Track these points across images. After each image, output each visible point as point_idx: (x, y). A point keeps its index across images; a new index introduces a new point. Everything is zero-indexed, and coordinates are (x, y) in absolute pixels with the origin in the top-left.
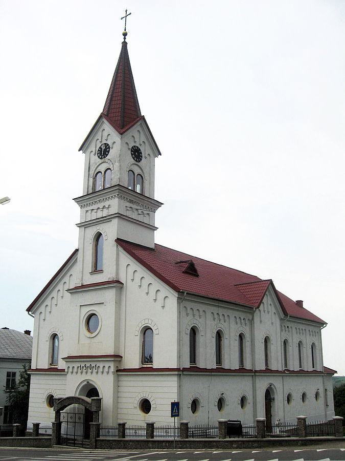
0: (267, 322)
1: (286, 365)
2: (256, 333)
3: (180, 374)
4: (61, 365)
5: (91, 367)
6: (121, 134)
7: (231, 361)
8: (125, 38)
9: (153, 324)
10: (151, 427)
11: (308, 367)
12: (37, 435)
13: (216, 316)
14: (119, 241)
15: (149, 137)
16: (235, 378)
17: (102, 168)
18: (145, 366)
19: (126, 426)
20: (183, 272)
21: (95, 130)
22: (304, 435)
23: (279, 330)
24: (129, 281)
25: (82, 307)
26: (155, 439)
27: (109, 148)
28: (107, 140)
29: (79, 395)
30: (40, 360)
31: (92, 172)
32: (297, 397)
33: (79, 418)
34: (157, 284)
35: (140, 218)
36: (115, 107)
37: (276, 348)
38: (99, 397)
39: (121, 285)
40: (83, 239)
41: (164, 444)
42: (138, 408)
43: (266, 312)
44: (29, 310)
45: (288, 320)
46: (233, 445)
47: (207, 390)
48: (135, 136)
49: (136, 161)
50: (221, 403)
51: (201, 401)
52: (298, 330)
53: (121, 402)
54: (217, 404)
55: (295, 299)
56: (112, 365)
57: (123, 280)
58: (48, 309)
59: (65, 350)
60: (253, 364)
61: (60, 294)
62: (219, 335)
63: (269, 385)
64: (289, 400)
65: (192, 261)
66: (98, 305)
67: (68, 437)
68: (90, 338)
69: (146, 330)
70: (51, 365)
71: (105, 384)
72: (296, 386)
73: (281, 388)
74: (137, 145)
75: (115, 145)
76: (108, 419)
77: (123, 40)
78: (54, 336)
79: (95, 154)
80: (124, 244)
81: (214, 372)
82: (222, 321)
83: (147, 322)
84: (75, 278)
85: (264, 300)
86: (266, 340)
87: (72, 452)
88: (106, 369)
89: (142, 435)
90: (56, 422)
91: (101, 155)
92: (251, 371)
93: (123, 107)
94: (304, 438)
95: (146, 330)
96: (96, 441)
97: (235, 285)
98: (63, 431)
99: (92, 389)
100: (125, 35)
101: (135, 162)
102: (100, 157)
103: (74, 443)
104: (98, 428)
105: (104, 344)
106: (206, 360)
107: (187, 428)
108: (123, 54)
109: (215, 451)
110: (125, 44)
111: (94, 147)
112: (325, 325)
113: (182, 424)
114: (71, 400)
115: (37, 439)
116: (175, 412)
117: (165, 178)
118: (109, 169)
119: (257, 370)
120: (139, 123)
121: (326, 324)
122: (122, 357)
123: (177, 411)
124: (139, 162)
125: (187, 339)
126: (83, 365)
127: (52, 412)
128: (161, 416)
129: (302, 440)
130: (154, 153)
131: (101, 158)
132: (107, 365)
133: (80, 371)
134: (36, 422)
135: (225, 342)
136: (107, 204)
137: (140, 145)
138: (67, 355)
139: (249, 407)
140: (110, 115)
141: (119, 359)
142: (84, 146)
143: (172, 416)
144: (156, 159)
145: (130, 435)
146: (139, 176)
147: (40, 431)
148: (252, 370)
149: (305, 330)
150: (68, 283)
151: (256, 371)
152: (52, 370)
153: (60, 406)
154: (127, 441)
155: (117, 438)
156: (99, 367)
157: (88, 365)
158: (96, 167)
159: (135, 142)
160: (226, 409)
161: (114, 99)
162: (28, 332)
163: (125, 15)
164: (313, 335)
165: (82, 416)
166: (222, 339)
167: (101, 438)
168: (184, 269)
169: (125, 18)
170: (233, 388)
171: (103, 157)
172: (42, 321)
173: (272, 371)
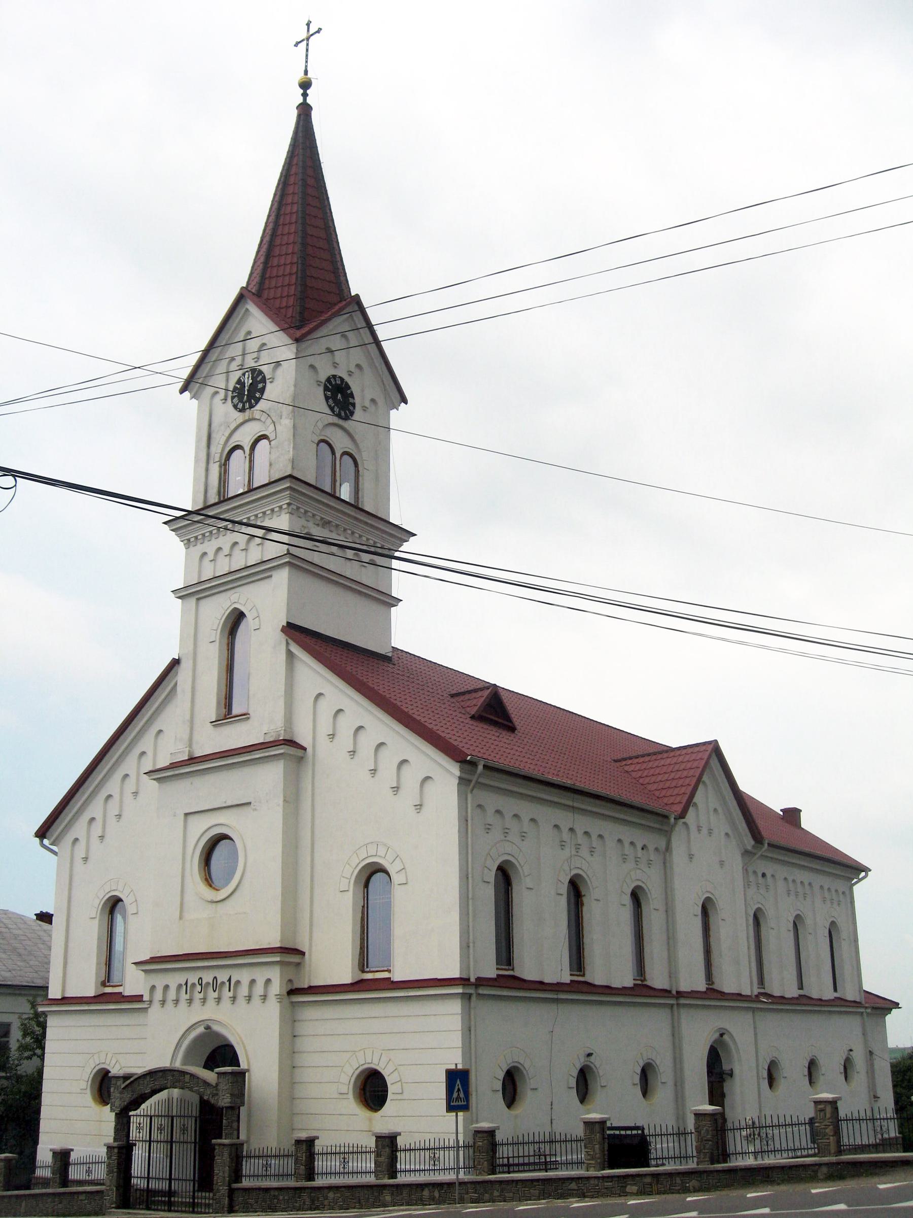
0: (704, 860)
1: (761, 981)
2: (678, 884)
3: (470, 995)
4: (133, 982)
5: (216, 985)
6: (297, 340)
7: (611, 964)
8: (305, 95)
9: (390, 857)
11: (820, 986)
13: (566, 835)
14: (293, 630)
15: (379, 361)
17: (245, 437)
18: (369, 976)
19: (318, 1146)
20: (473, 717)
22: (833, 1148)
24: (322, 740)
25: (191, 819)
26: (401, 1179)
27: (264, 380)
29: (185, 1061)
30: (73, 971)
31: (217, 450)
33: (184, 1130)
34: (402, 744)
35: (351, 570)
36: (284, 248)
37: (733, 932)
38: (239, 1066)
39: (299, 753)
40: (192, 632)
41: (426, 1193)
42: (351, 1096)
43: (705, 831)
44: (41, 834)
45: (763, 857)
46: (629, 1189)
47: (549, 1042)
48: (336, 353)
49: (339, 416)
50: (584, 1083)
51: (527, 1064)
52: (791, 885)
53: (306, 1083)
54: (573, 1082)
55: (777, 806)
56: (275, 975)
58: (97, 829)
59: (140, 938)
60: (672, 974)
61: (130, 785)
62: (576, 890)
63: (717, 1035)
64: (771, 1081)
66: (235, 810)
67: (154, 1185)
68: (212, 902)
69: (371, 874)
71: (254, 1028)
72: (792, 1040)
73: (752, 1041)
75: (280, 371)
76: (264, 1132)
77: (301, 100)
78: (114, 905)
79: (226, 399)
80: (308, 640)
81: (563, 991)
82: (584, 852)
83: (372, 851)
84: (167, 742)
85: (698, 798)
86: (707, 909)
88: (259, 989)
89: (364, 1170)
90: (116, 1144)
91: (241, 401)
92: (665, 993)
93: (300, 268)
94: (833, 1159)
96: (231, 1192)
97: (615, 761)
99: (219, 1047)
100: (305, 85)
101: (335, 420)
102: (240, 406)
104: (237, 1156)
105: (251, 917)
106: (542, 954)
107: (311, 1156)
108: (300, 134)
109: (577, 1202)
110: (305, 111)
111: (225, 377)
112: (863, 874)
113: (477, 1132)
114: (158, 1079)
115: (64, 1193)
116: (458, 1098)
117: (422, 469)
118: (264, 437)
121: (866, 870)
122: (303, 954)
123: (462, 1095)
125: (487, 894)
126: (193, 978)
127: (107, 1117)
128: (421, 1117)
131: (242, 410)
132: (261, 976)
133: (184, 997)
134: (58, 1146)
135: (592, 911)
137: (350, 373)
138: (144, 954)
139: (663, 1094)
140: (266, 292)
141: (295, 959)
143: (450, 1108)
144: (393, 413)
145: (328, 1170)
146: (346, 457)
147: (74, 1173)
149: (810, 884)
150: (150, 754)
151: (680, 994)
152: (109, 998)
153: (128, 1097)
154: (320, 1189)
155: (292, 1183)
156: (238, 982)
157: (208, 977)
158: (227, 434)
159: (335, 365)
160: (599, 1097)
161: (277, 251)
162: (45, 917)
163: (304, 36)
165: (191, 1124)
166: (585, 900)
167: (246, 1183)
168: (473, 711)
169: (305, 42)
170: (620, 1040)
171: (247, 405)
173: (722, 996)
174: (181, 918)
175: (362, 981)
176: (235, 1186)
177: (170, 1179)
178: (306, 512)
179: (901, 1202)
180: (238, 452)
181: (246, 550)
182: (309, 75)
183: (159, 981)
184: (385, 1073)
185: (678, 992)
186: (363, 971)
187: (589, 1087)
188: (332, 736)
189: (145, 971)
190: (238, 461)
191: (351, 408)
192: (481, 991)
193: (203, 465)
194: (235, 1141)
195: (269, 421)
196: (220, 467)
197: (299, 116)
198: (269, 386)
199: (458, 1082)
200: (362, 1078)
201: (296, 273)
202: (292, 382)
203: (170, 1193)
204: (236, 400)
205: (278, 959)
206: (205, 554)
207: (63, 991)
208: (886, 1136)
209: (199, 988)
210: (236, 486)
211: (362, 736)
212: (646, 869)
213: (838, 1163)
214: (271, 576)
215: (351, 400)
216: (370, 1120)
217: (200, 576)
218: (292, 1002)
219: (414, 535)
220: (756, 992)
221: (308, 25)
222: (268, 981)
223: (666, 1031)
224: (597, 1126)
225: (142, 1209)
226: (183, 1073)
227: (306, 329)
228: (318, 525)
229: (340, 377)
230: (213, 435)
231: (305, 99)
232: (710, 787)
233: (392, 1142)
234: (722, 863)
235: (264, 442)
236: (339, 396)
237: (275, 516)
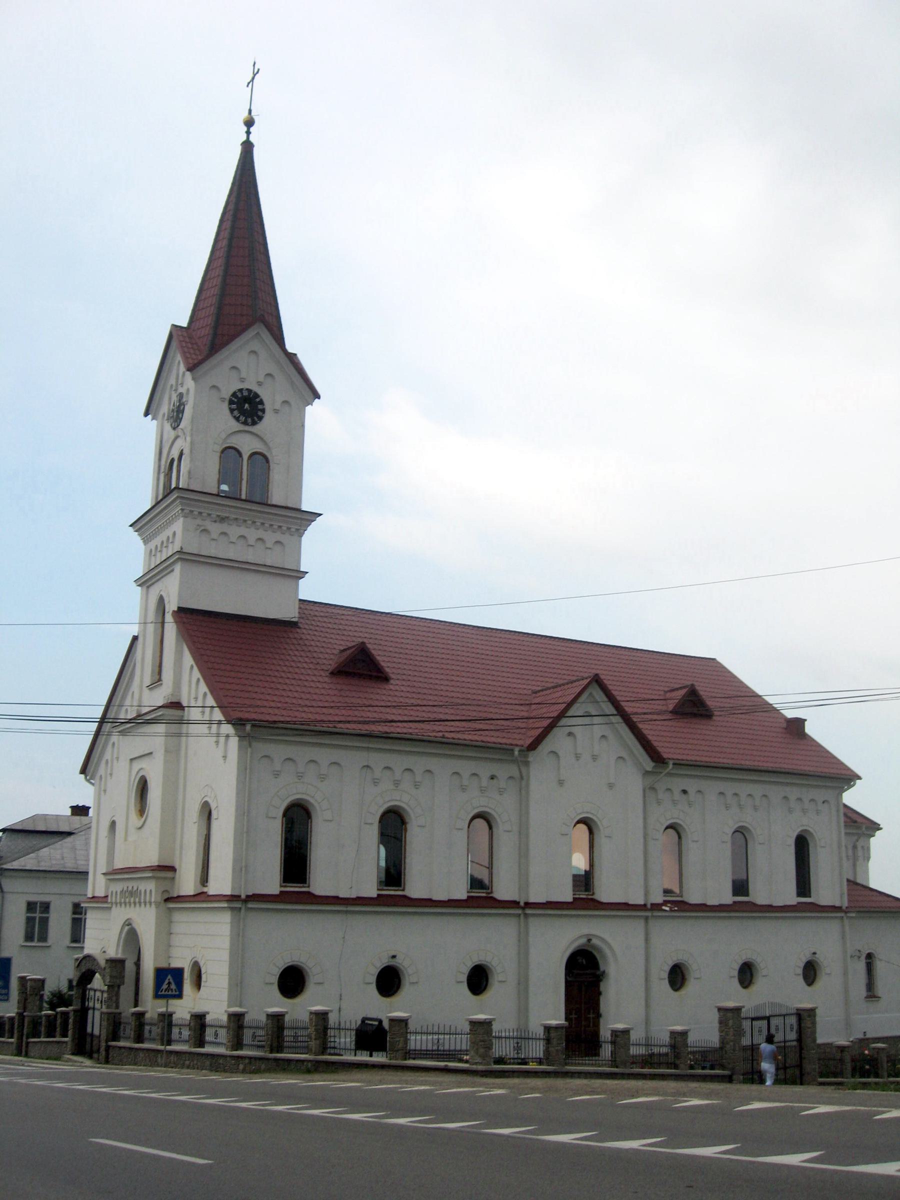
8: (248, 133)
16: (491, 919)
44: (83, 771)
45: (669, 774)
48: (242, 366)
49: (245, 423)
71: (146, 921)
77: (244, 138)
92: (514, 904)
93: (238, 292)
96: (108, 1048)
107: (170, 1025)
110: (247, 148)
121: (859, 778)
123: (173, 986)
124: (254, 423)
141: (169, 874)
144: (308, 409)
148: (519, 903)
182: (253, 114)
183: (117, 887)
191: (260, 413)
192: (250, 905)
194: (113, 1010)
199: (169, 977)
208: (441, 1048)
214: (172, 571)
215: (260, 407)
218: (169, 908)
219: (320, 515)
228: (215, 521)
234: (611, 786)
236: (247, 406)
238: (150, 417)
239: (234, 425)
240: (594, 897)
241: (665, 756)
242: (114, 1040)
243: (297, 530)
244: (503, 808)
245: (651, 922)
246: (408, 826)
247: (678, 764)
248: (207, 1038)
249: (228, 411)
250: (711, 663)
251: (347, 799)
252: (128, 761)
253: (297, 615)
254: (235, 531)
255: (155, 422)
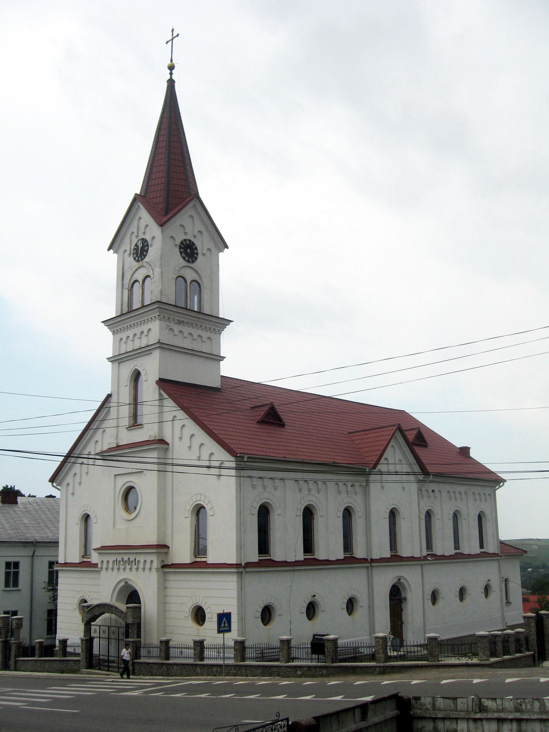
3: (242, 572)
4: (95, 558)
5: (129, 562)
6: (161, 225)
8: (171, 74)
9: (206, 501)
10: (200, 645)
12: (65, 656)
17: (140, 276)
18: (199, 560)
19: (171, 643)
20: (258, 422)
21: (128, 220)
23: (415, 497)
25: (118, 478)
26: (206, 662)
27: (147, 245)
28: (144, 233)
30: (69, 551)
31: (126, 282)
32: (449, 595)
35: (196, 346)
36: (158, 170)
39: (165, 446)
40: (117, 380)
41: (215, 669)
42: (190, 618)
44: (52, 480)
45: (431, 482)
47: (288, 592)
48: (185, 225)
49: (188, 261)
50: (311, 610)
53: (175, 611)
55: (459, 444)
56: (154, 558)
57: (168, 440)
58: (77, 479)
62: (308, 514)
63: (396, 580)
65: (272, 403)
68: (127, 520)
70: (83, 557)
71: (146, 583)
72: (447, 579)
74: (189, 237)
76: (152, 636)
77: (169, 77)
82: (314, 492)
84: (105, 440)
86: (393, 514)
87: (93, 681)
88: (148, 565)
90: (85, 638)
91: (137, 256)
92: (364, 560)
93: (171, 182)
94: (382, 664)
95: (199, 510)
98: (96, 651)
100: (171, 68)
101: (187, 264)
102: (137, 259)
103: (109, 667)
105: (144, 531)
107: (289, 648)
110: (171, 83)
111: (128, 245)
112: (502, 484)
114: (103, 608)
116: (224, 627)
117: (236, 278)
119: (374, 558)
120: (191, 205)
123: (227, 625)
124: (193, 262)
129: (380, 667)
130: (216, 245)
131: (138, 261)
132: (149, 558)
136: (145, 328)
137: (195, 236)
139: (361, 612)
141: (165, 550)
142: (115, 242)
143: (219, 631)
144: (221, 254)
147: (69, 650)
151: (372, 561)
152: (85, 565)
153: (89, 616)
154: (170, 664)
157: (126, 558)
159: (185, 233)
160: (320, 617)
163: (170, 38)
164: (481, 500)
167: (142, 660)
168: (259, 418)
170: (331, 588)
171: (140, 259)
172: (70, 495)
173: (401, 559)
174: (114, 527)
175: (196, 562)
176: (135, 661)
177: (108, 656)
178: (169, 318)
179: (419, 683)
180: (137, 283)
181: (140, 338)
183: (105, 558)
184: (204, 608)
185: (371, 560)
186: (196, 557)
187: (316, 611)
188: (181, 438)
189: (99, 553)
190: (137, 288)
191: (196, 256)
193: (120, 290)
195: (150, 268)
196: (129, 291)
197: (168, 87)
198: (150, 249)
199: (224, 619)
200: (196, 609)
201: (164, 183)
202: (160, 248)
203: (109, 661)
204: (135, 255)
205: (155, 551)
206: (121, 339)
207: (65, 559)
209: (122, 563)
210: (136, 304)
211: (194, 439)
212: (354, 497)
213: (384, 667)
215: (196, 251)
216: (198, 630)
217: (119, 351)
218: (164, 572)
220: (425, 553)
221: (172, 31)
222: (152, 561)
223: (365, 581)
224: (285, 643)
225: (97, 669)
226: (112, 606)
227: (170, 215)
229: (189, 240)
230: (125, 274)
231: (171, 77)
232: (396, 447)
233: (201, 644)
235: (148, 279)
236: (188, 250)
237: (153, 322)
238: (111, 251)
239: (183, 263)
240: (398, 554)
241: (430, 471)
242: (136, 659)
243: (219, 330)
244: (358, 505)
245: (424, 567)
246: (315, 517)
247: (437, 475)
248: (142, 654)
249: (179, 254)
250: (403, 412)
251: (288, 499)
252: (113, 476)
253: (220, 384)
254: (187, 330)
255: (116, 255)
